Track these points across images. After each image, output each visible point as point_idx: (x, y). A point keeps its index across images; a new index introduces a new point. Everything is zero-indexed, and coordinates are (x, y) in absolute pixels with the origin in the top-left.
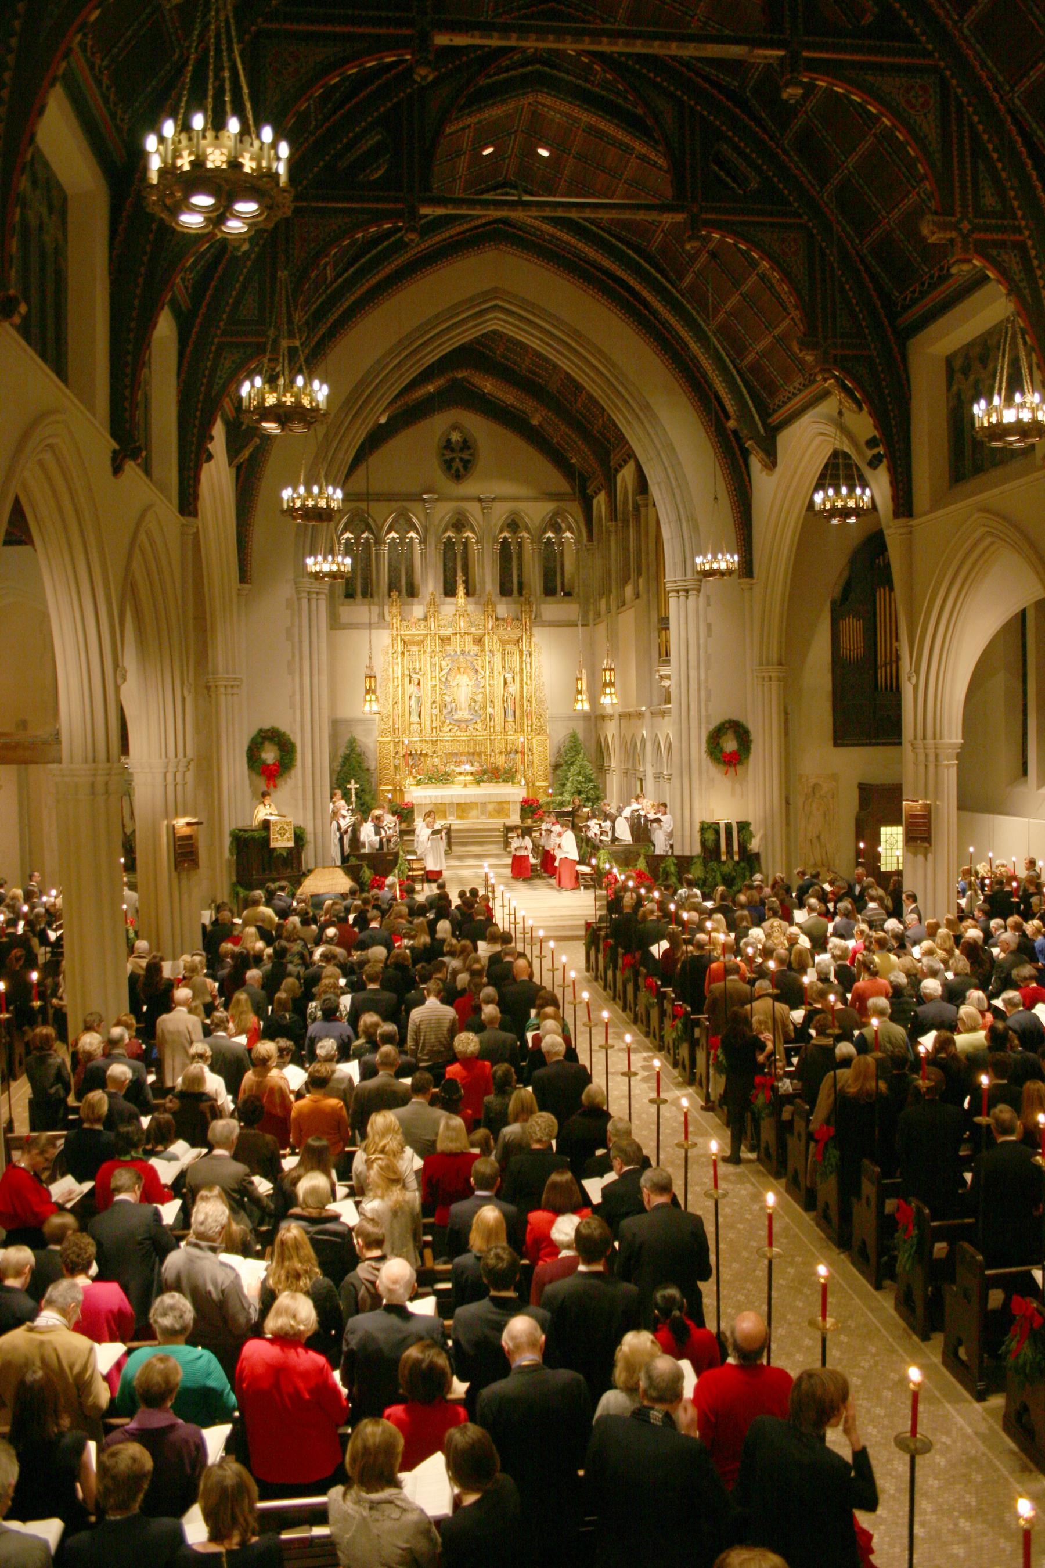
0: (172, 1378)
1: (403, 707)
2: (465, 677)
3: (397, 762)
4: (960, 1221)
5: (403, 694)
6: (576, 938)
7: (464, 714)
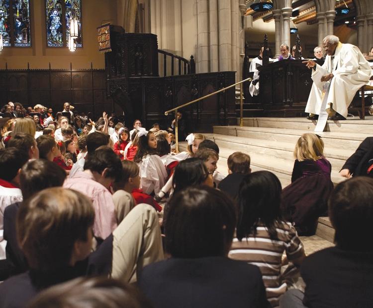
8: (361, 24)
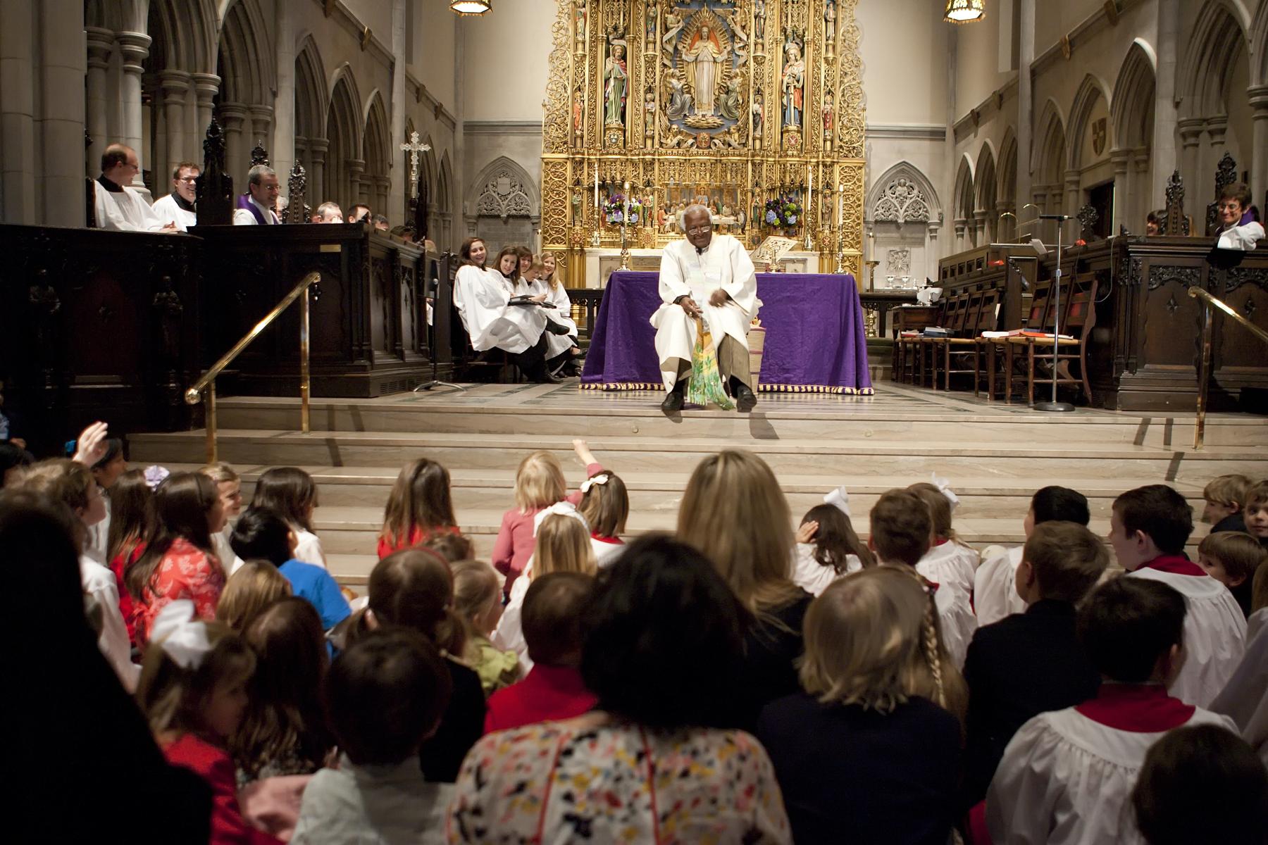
0: (288, 588)
1: (593, 97)
2: (711, 46)
3: (576, 199)
4: (305, 364)
5: (593, 76)
6: (44, 218)
7: (705, 113)
8: (234, 126)
